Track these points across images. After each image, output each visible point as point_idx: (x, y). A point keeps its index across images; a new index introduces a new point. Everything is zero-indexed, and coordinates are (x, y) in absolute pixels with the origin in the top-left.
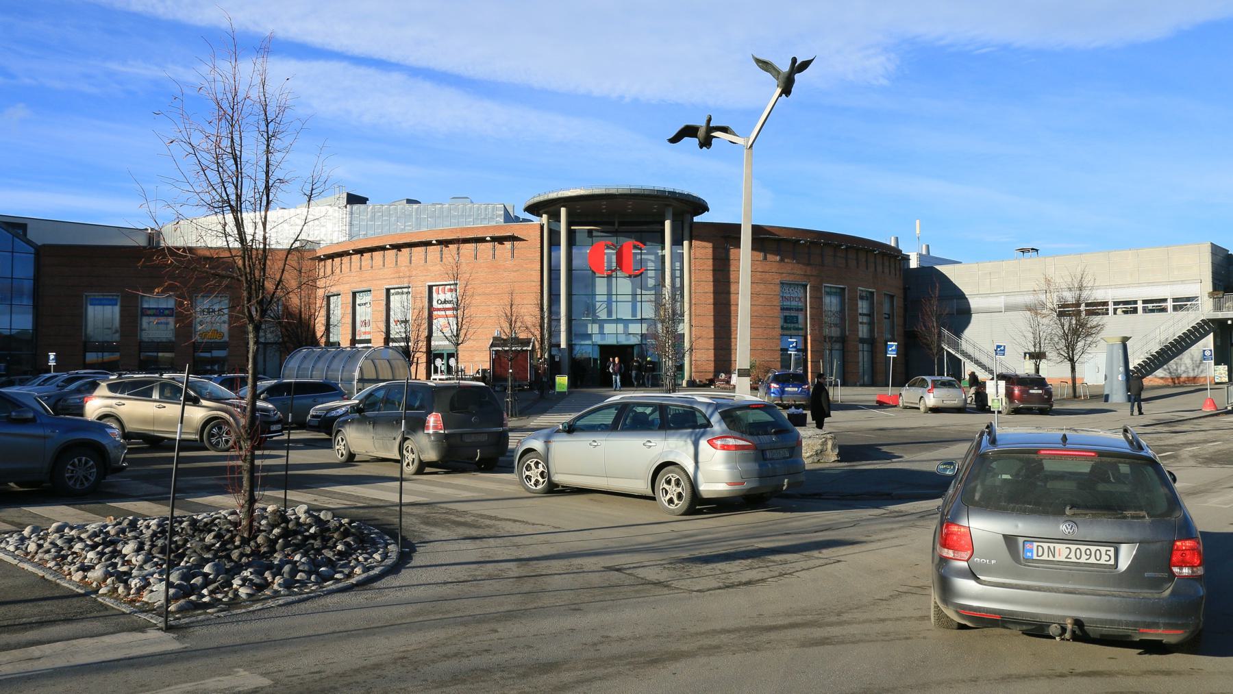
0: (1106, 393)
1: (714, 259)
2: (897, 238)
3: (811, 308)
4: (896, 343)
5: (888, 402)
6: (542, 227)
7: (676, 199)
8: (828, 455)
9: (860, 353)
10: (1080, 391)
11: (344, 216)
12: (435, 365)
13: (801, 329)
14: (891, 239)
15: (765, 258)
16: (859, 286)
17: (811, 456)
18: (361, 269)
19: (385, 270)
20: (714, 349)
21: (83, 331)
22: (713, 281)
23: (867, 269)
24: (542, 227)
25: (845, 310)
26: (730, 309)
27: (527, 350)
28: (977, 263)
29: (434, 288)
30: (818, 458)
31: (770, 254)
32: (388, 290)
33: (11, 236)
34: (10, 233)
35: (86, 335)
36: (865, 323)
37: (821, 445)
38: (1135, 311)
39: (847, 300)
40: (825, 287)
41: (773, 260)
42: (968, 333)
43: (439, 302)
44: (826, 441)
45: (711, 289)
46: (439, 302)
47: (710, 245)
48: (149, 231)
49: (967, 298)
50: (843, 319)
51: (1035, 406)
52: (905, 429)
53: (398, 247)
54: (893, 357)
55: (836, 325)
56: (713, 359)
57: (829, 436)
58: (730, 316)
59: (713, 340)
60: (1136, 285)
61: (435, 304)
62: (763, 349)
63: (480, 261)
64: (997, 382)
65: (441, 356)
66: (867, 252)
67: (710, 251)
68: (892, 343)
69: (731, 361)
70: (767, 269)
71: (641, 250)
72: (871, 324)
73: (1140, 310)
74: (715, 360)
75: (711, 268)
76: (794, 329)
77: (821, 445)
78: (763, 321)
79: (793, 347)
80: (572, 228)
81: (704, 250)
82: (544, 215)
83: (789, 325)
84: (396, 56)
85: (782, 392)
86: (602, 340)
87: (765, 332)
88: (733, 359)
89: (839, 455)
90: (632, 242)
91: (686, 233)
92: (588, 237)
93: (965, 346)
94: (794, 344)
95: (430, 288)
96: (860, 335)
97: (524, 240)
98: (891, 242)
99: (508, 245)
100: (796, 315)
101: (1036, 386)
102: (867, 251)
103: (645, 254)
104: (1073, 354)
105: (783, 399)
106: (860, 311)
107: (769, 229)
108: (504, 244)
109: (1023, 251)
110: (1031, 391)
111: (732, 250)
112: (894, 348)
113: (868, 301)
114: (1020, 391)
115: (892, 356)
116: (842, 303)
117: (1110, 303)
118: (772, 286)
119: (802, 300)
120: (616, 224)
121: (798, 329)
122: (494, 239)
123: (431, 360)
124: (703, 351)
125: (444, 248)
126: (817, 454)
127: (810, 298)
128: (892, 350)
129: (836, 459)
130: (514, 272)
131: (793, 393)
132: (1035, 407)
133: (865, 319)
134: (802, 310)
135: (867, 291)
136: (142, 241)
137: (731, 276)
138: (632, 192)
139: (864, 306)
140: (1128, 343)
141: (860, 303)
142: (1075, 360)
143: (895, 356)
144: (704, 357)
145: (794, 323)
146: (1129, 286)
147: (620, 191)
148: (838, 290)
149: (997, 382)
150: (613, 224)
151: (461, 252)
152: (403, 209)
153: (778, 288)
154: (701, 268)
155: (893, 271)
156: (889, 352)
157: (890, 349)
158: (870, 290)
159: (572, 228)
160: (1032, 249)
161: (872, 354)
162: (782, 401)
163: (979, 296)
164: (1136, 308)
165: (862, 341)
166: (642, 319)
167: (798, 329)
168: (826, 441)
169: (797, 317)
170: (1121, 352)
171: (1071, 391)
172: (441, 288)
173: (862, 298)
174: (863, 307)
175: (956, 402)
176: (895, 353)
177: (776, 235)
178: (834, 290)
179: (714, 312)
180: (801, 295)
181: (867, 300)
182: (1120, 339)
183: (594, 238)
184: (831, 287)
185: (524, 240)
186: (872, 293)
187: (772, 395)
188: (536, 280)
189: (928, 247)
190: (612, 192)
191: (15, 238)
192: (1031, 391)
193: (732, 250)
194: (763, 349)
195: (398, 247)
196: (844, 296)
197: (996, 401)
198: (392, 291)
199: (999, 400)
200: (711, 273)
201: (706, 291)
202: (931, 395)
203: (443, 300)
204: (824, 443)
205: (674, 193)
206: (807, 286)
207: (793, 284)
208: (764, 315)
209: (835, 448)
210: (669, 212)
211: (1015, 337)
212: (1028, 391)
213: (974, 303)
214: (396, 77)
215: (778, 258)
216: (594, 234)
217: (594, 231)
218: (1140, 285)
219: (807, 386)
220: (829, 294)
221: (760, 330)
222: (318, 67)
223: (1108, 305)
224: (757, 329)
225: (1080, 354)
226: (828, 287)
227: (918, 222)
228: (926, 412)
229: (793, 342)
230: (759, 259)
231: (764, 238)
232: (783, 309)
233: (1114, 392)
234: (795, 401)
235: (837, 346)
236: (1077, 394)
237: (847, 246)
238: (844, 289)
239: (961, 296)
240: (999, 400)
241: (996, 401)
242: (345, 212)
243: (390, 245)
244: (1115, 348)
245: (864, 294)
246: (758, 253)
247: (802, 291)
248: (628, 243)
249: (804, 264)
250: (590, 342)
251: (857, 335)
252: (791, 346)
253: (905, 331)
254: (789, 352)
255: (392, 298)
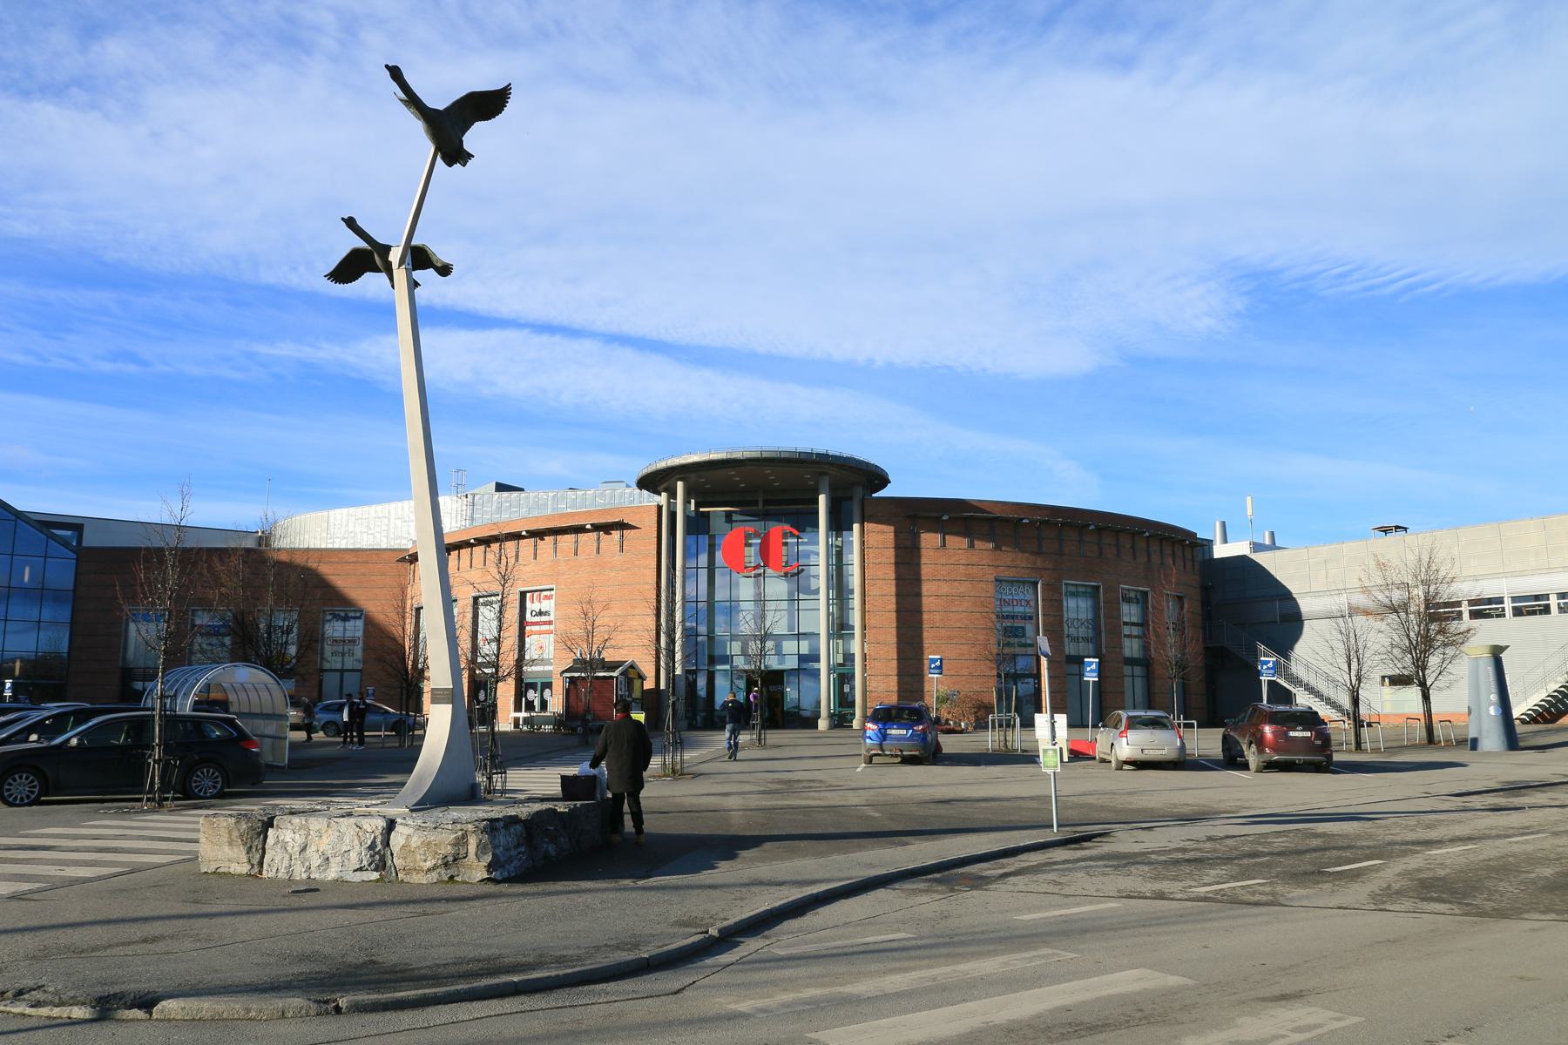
0: (1472, 735)
1: (897, 548)
2: (1224, 523)
3: (1043, 615)
4: (1097, 660)
5: (1087, 752)
6: (660, 508)
7: (831, 464)
8: (470, 867)
9: (1128, 681)
10: (1439, 732)
11: (464, 508)
12: (526, 699)
13: (1031, 645)
14: (1264, 534)
15: (972, 546)
16: (1120, 584)
17: (434, 868)
18: (458, 570)
19: (473, 573)
20: (899, 675)
21: (121, 655)
22: (896, 579)
23: (1134, 559)
24: (660, 508)
25: (1099, 617)
26: (921, 618)
27: (612, 677)
28: (1306, 547)
29: (528, 595)
30: (450, 873)
31: (979, 539)
32: (476, 599)
33: (45, 537)
34: (44, 534)
35: (124, 659)
36: (1136, 637)
37: (454, 845)
38: (1546, 610)
39: (1102, 604)
40: (1066, 584)
41: (984, 547)
42: (1301, 649)
43: (534, 613)
44: (464, 836)
45: (893, 590)
46: (534, 613)
47: (892, 528)
48: (260, 534)
49: (1294, 599)
50: (1097, 629)
51: (1299, 758)
52: (847, 806)
53: (486, 541)
54: (1093, 681)
55: (1086, 640)
56: (896, 689)
57: (470, 827)
58: (921, 628)
59: (895, 662)
60: (1545, 571)
61: (529, 617)
62: (970, 674)
63: (581, 557)
64: (1052, 717)
65: (533, 686)
66: (1173, 543)
67: (891, 536)
68: (1091, 660)
69: (923, 691)
70: (975, 560)
71: (798, 537)
72: (1143, 637)
73: (1554, 608)
74: (898, 691)
75: (893, 561)
76: (1019, 646)
77: (454, 845)
78: (970, 635)
79: (936, 667)
80: (701, 509)
81: (882, 536)
82: (663, 494)
83: (1012, 640)
84: (578, 320)
85: (884, 736)
86: (781, 663)
87: (973, 650)
88: (926, 689)
89: (490, 867)
90: (787, 527)
91: (856, 512)
92: (726, 522)
93: (1297, 669)
94: (938, 663)
95: (523, 594)
96: (1127, 653)
97: (638, 528)
98: (1264, 540)
99: (616, 534)
100: (1023, 625)
101: (1300, 725)
102: (1134, 534)
103: (805, 543)
104: (1424, 675)
105: (885, 747)
106: (1126, 619)
107: (978, 504)
108: (611, 534)
109: (1385, 530)
110: (1292, 734)
111: (922, 535)
112: (1094, 667)
113: (1140, 605)
114: (1273, 733)
115: (1091, 679)
116: (1096, 608)
117: (1505, 599)
118: (982, 585)
119: (1032, 603)
120: (760, 504)
121: (1026, 645)
122: (597, 528)
123: (522, 692)
124: (879, 677)
125: (539, 541)
126: (446, 865)
127: (1043, 600)
128: (1092, 671)
129: (486, 876)
130: (623, 571)
131: (899, 738)
132: (1300, 760)
133: (1135, 631)
134: (1031, 618)
135: (1137, 591)
136: (250, 543)
137: (923, 572)
138: (763, 456)
139: (1132, 612)
140: (1504, 656)
141: (1125, 608)
142: (1428, 683)
143: (1097, 679)
144: (882, 687)
145: (1017, 636)
146: (1533, 573)
147: (747, 455)
148: (1089, 590)
149: (1052, 717)
150: (755, 503)
151: (559, 545)
152: (535, 497)
153: (992, 588)
154: (878, 561)
155: (1189, 564)
156: (1087, 674)
157: (1088, 669)
158: (1141, 588)
159: (701, 509)
160: (1397, 527)
161: (1148, 681)
162: (882, 750)
163: (1311, 594)
164: (1548, 606)
165: (1130, 661)
166: (799, 634)
167: (1026, 645)
168: (464, 836)
169: (1023, 628)
170: (1490, 671)
171: (1424, 734)
172: (535, 594)
173: (1128, 600)
174: (1130, 613)
175: (1163, 752)
176: (1095, 674)
177: (990, 513)
178: (1082, 589)
179: (897, 622)
180: (1029, 596)
181: (1138, 603)
182: (1488, 650)
183: (734, 524)
184: (1076, 585)
185: (638, 528)
186: (1145, 594)
187: (868, 741)
188: (650, 582)
189: (1272, 534)
190: (738, 456)
191: (50, 540)
192: (1292, 734)
193: (922, 535)
194: (970, 674)
195: (486, 541)
196: (1098, 598)
197: (1051, 753)
198: (481, 600)
199: (1055, 750)
200: (893, 568)
201: (884, 592)
202: (1124, 740)
203: (538, 611)
204: (461, 841)
205: (826, 455)
206: (1037, 583)
207: (1016, 581)
208: (971, 626)
209: (484, 853)
210: (825, 483)
211: (1318, 650)
212: (1286, 734)
213: (1306, 605)
214: (587, 345)
215: (991, 545)
216: (735, 517)
217: (734, 515)
218: (1550, 570)
219: (921, 727)
220: (1075, 595)
221: (965, 647)
222: (494, 336)
223: (1502, 603)
224: (961, 646)
225: (1435, 675)
226: (1073, 585)
227: (1249, 499)
228: (1119, 768)
229: (936, 660)
230: (963, 547)
231: (967, 518)
232: (1001, 617)
233: (1484, 733)
234: (901, 751)
235: (1138, 670)
236: (1436, 739)
237: (1097, 526)
238: (1097, 588)
239: (1286, 596)
240: (1055, 750)
241: (1051, 753)
242: (465, 503)
243: (474, 539)
244: (1481, 663)
245: (1132, 595)
246: (961, 539)
247: (1031, 591)
248: (777, 528)
249: (1032, 553)
250: (728, 667)
251: (1064, 651)
252: (933, 666)
253: (1207, 649)
254: (1085, 679)
255: (482, 609)
